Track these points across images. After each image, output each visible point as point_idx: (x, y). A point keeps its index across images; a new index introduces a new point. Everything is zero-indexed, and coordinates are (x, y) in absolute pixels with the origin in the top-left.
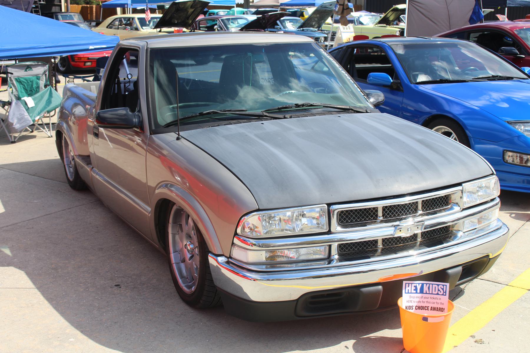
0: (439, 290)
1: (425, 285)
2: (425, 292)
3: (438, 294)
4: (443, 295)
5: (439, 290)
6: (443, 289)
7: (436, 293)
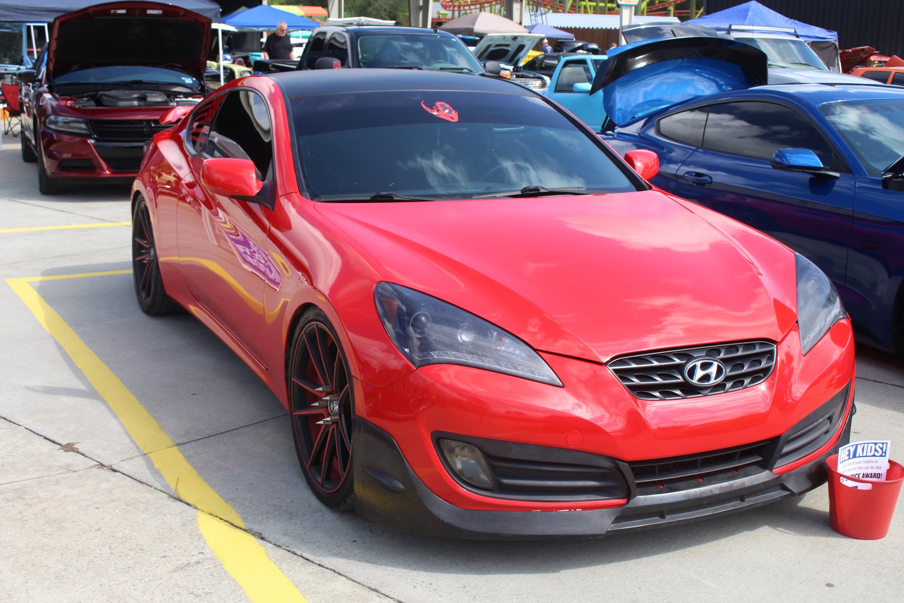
3: (874, 455)
4: (881, 456)
5: (876, 450)
6: (882, 449)
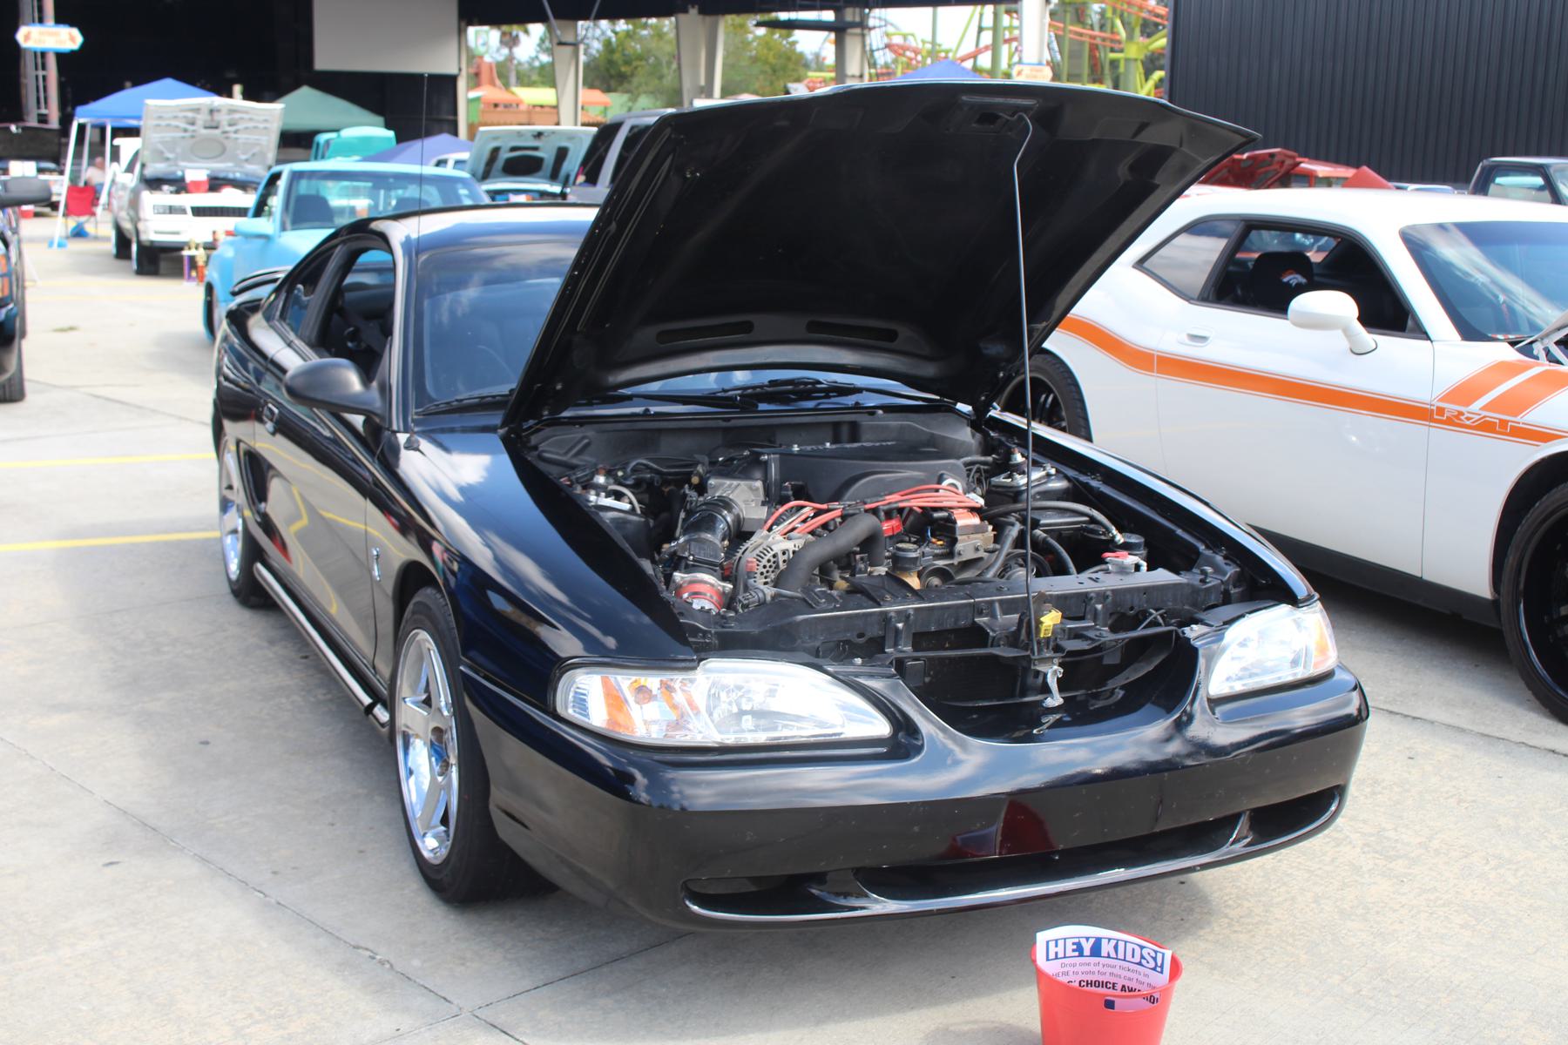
0: (1142, 957)
1: (1104, 942)
2: (1104, 953)
3: (1140, 964)
5: (1142, 957)
6: (1155, 959)
7: (1137, 959)
